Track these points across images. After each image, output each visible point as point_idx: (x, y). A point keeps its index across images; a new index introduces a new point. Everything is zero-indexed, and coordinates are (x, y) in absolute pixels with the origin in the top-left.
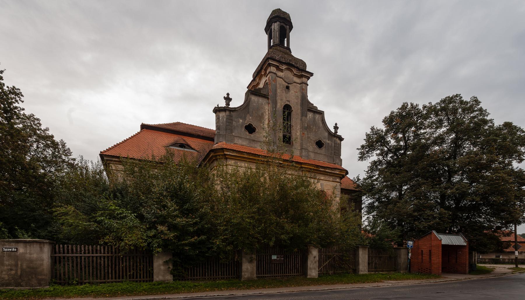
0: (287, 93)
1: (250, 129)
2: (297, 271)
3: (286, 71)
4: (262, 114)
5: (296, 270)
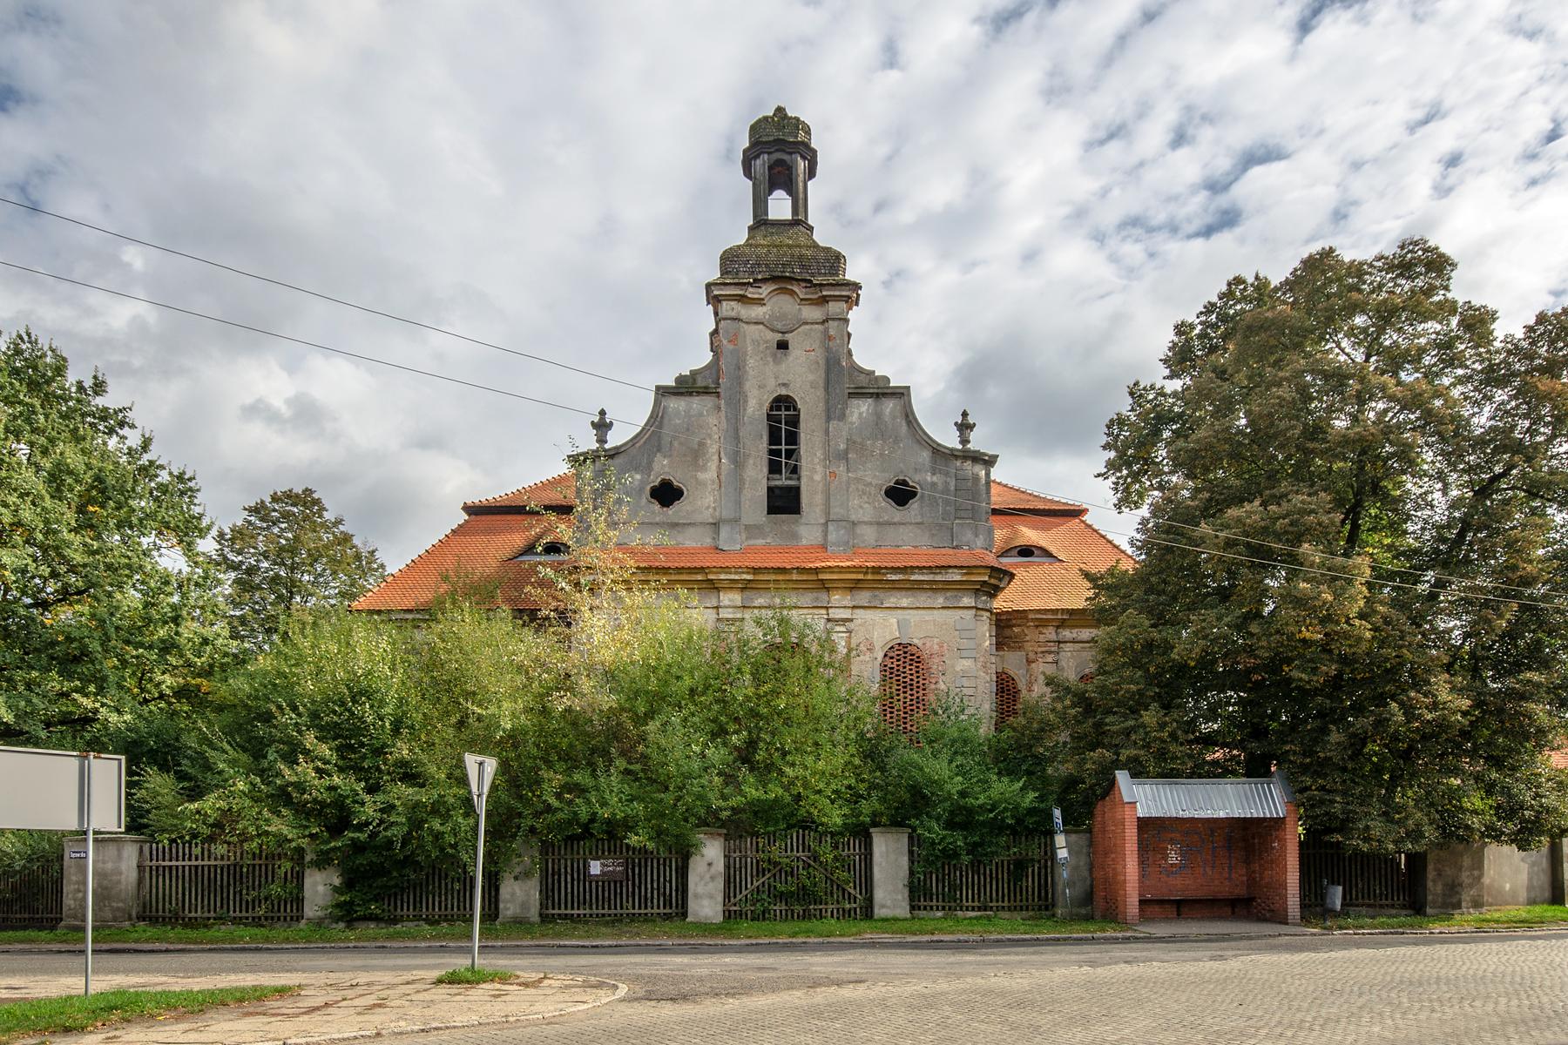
0: (776, 361)
1: (666, 494)
2: (668, 903)
3: (775, 299)
4: (701, 444)
5: (662, 899)
